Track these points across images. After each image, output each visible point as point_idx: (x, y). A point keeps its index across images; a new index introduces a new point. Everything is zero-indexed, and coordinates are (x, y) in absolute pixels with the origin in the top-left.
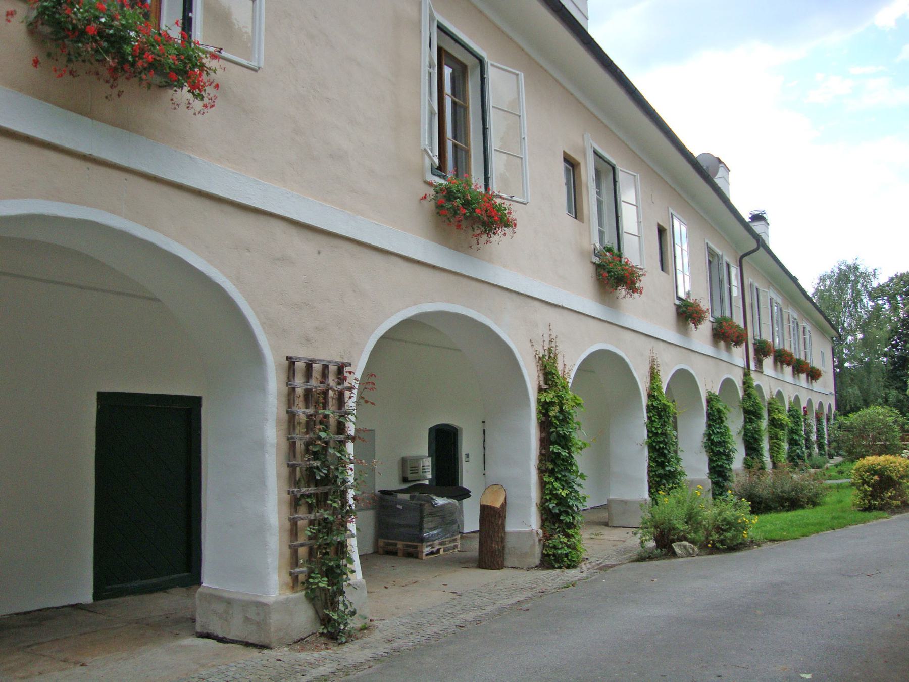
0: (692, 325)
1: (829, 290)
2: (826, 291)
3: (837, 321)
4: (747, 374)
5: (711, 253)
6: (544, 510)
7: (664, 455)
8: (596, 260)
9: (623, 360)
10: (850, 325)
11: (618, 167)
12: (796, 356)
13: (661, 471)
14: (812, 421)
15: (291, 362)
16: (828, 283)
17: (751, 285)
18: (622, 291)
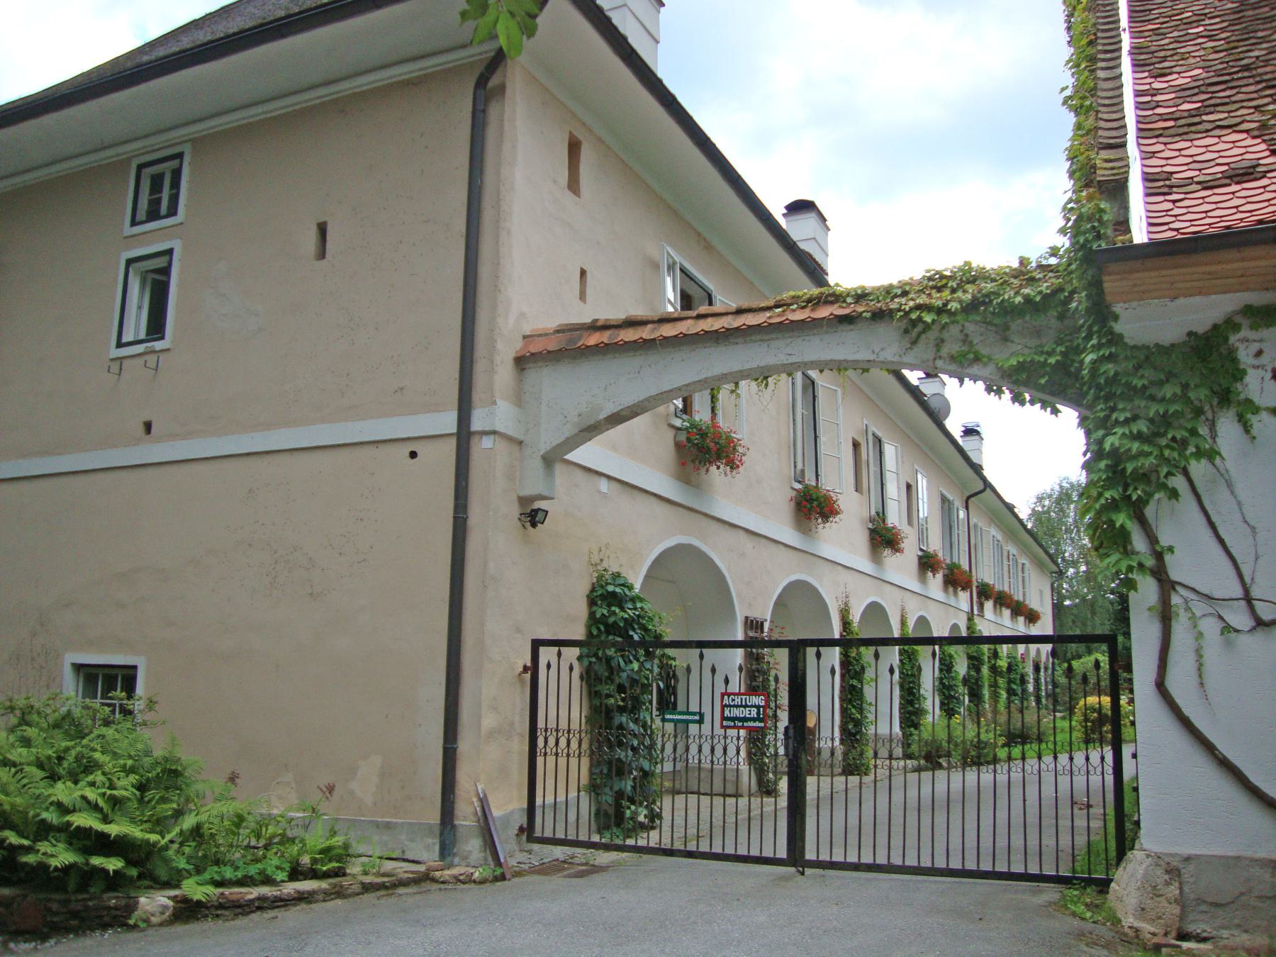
0: (930, 574)
1: (1048, 512)
2: (1044, 513)
3: (1057, 550)
4: (970, 619)
5: (944, 499)
6: (844, 729)
7: (914, 694)
8: (870, 526)
9: (723, 576)
10: (1072, 555)
11: (883, 440)
12: (998, 588)
13: (910, 708)
14: (1029, 670)
15: (747, 618)
16: (1047, 503)
17: (976, 526)
18: (887, 552)
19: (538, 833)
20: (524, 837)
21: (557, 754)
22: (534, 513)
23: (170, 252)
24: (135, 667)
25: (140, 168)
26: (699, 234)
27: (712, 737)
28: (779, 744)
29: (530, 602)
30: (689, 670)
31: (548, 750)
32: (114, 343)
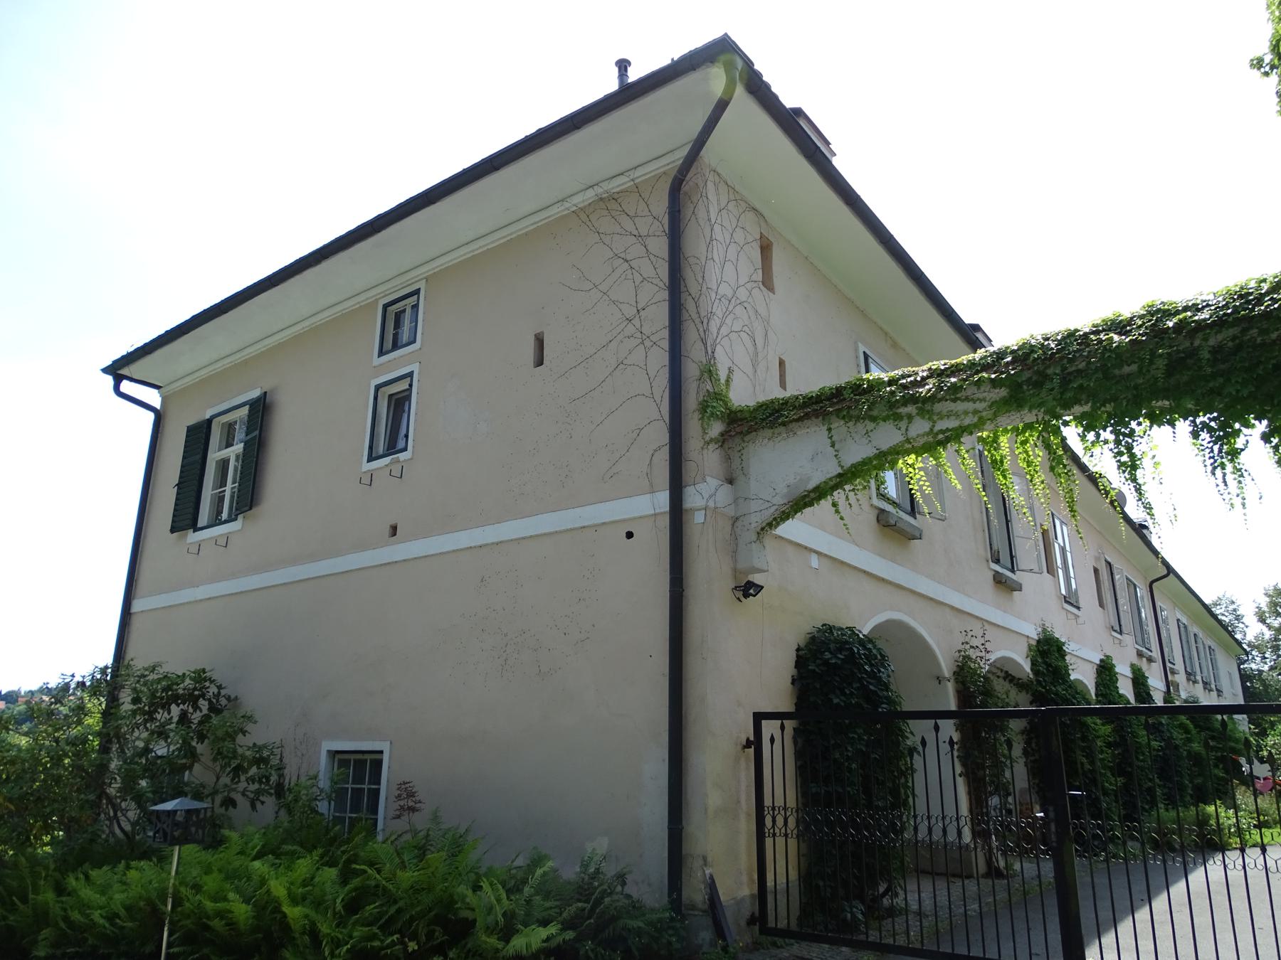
19: (771, 924)
20: (757, 928)
21: (774, 835)
22: (750, 585)
23: (411, 375)
24: (382, 752)
25: (386, 307)
26: (886, 334)
27: (943, 818)
28: (962, 822)
29: (747, 670)
30: (924, 743)
31: (777, 831)
32: (365, 458)
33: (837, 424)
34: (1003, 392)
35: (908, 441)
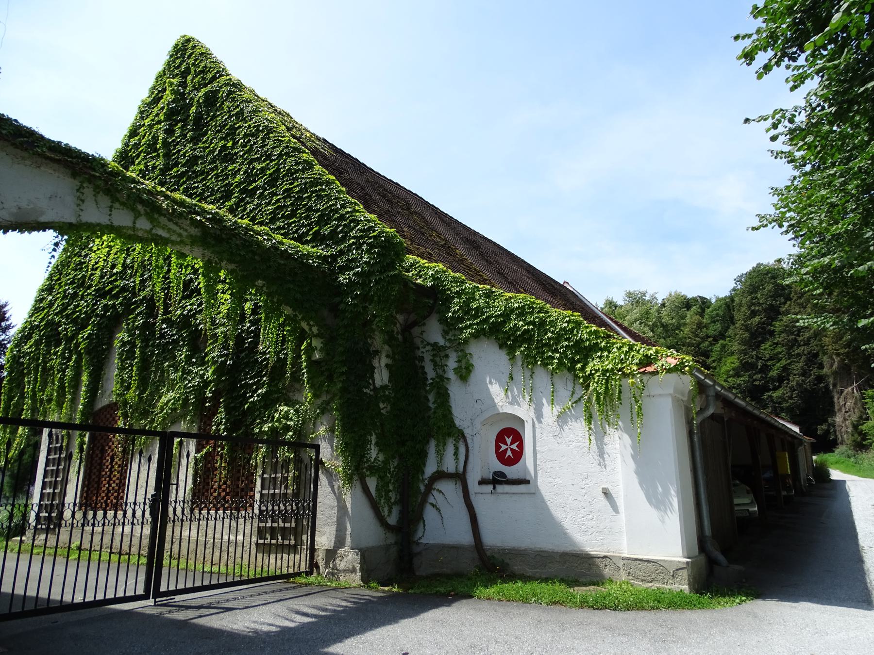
33: (89, 191)
34: (194, 231)
35: (134, 228)
